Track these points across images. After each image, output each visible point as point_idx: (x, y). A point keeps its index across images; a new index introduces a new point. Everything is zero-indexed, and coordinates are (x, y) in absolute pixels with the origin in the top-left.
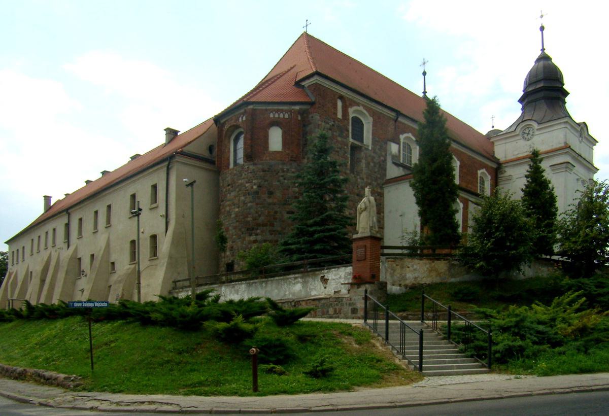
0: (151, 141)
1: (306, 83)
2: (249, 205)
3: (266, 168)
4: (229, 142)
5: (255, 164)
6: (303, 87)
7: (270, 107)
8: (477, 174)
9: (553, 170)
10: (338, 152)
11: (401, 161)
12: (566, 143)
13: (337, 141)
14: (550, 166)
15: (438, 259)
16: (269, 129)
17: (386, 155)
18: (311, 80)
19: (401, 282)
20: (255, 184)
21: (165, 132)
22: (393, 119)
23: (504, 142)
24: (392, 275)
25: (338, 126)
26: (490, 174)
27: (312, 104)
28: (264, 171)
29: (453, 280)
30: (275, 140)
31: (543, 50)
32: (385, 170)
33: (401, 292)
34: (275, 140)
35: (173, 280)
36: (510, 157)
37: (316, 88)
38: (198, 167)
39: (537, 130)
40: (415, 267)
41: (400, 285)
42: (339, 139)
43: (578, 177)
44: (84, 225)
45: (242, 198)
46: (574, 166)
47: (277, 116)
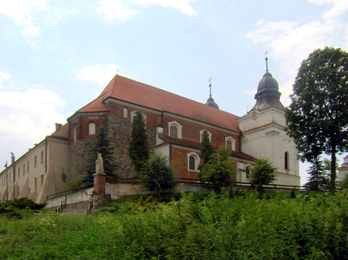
0: (52, 130)
1: (106, 102)
2: (80, 160)
3: (87, 143)
4: (74, 130)
5: (82, 141)
6: (105, 103)
7: (89, 114)
8: (225, 139)
9: (267, 135)
10: (124, 134)
11: (169, 135)
12: (273, 121)
13: (124, 129)
14: (266, 133)
15: (135, 184)
16: (89, 124)
17: (156, 133)
18: (108, 100)
19: (118, 195)
20: (82, 150)
21: (55, 125)
22: (160, 116)
23: (248, 120)
24: (114, 191)
25: (124, 122)
26: (234, 138)
27: (108, 112)
28: (86, 144)
29: (143, 193)
30: (92, 129)
31: (267, 70)
32: (155, 141)
33: (117, 199)
34: (92, 129)
35: (47, 196)
36: (247, 129)
37: (111, 104)
38: (62, 143)
39: (260, 114)
40: (124, 187)
41: (117, 196)
42: (125, 127)
43: (284, 138)
44: (20, 170)
45: (77, 157)
46: (279, 133)
47: (92, 118)
